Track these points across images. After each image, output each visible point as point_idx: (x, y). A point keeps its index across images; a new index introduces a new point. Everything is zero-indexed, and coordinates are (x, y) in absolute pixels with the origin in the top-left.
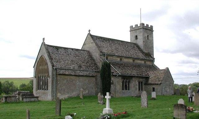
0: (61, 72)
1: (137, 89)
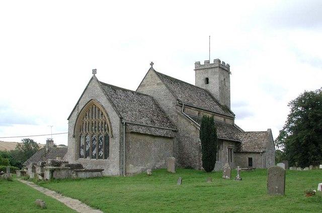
0: (135, 129)
1: (227, 160)
